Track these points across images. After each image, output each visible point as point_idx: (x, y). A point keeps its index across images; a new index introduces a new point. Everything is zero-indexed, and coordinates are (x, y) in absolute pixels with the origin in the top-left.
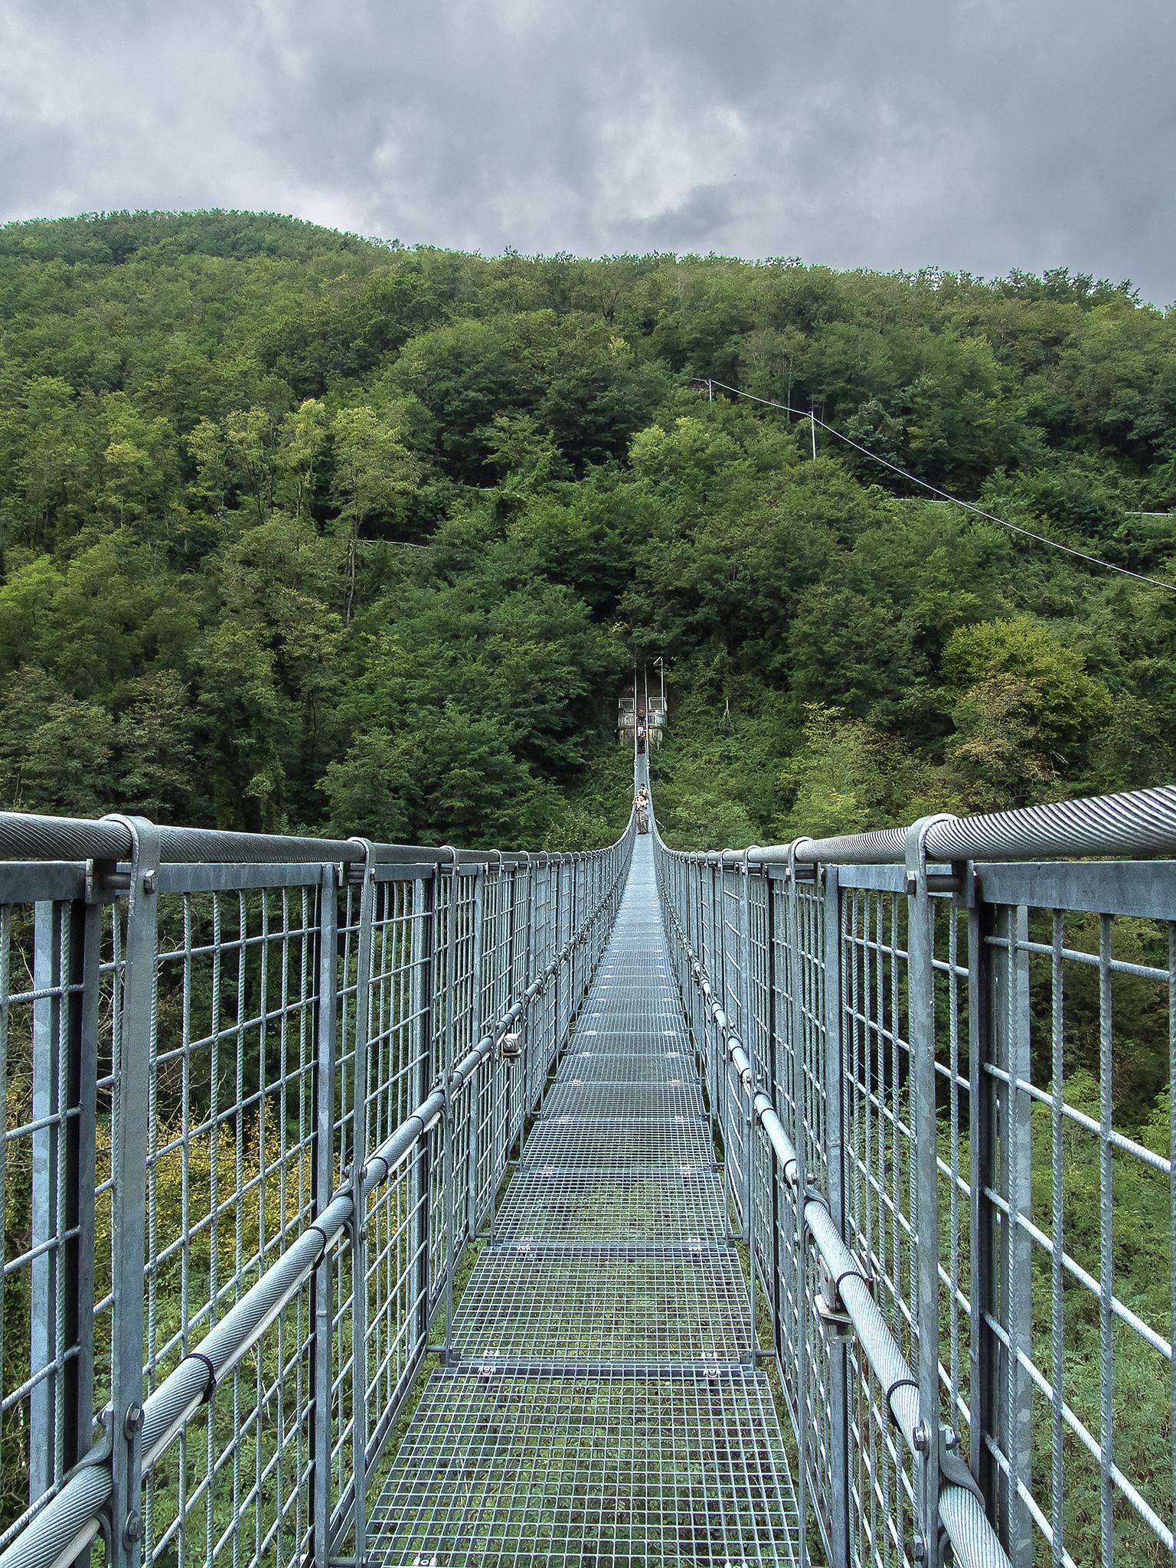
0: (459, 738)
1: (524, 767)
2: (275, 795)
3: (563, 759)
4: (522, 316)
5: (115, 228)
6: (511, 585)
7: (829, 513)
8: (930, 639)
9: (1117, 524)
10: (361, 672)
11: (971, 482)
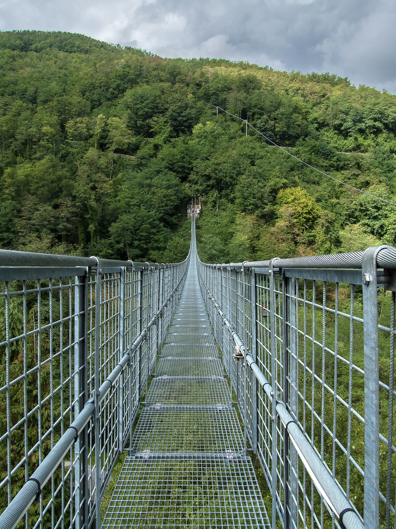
0: (145, 216)
1: (162, 224)
2: (95, 231)
3: (172, 222)
4: (161, 84)
5: (25, 36)
6: (158, 172)
7: (249, 153)
8: (274, 191)
9: (334, 156)
10: (116, 196)
11: (293, 141)
